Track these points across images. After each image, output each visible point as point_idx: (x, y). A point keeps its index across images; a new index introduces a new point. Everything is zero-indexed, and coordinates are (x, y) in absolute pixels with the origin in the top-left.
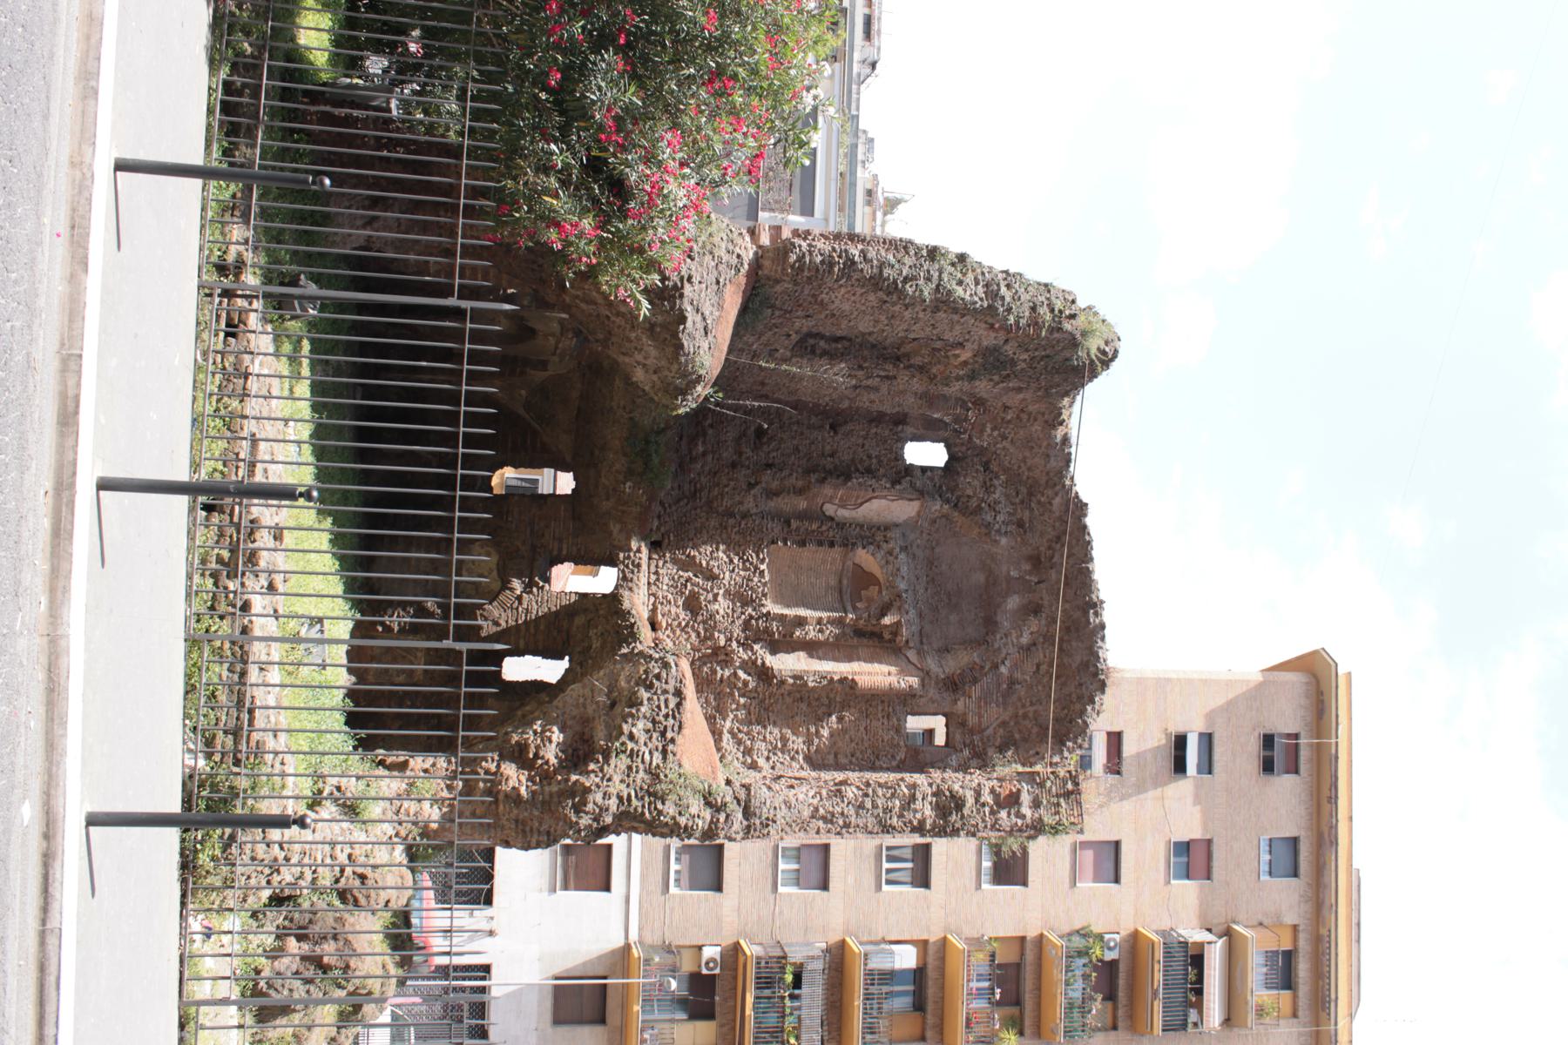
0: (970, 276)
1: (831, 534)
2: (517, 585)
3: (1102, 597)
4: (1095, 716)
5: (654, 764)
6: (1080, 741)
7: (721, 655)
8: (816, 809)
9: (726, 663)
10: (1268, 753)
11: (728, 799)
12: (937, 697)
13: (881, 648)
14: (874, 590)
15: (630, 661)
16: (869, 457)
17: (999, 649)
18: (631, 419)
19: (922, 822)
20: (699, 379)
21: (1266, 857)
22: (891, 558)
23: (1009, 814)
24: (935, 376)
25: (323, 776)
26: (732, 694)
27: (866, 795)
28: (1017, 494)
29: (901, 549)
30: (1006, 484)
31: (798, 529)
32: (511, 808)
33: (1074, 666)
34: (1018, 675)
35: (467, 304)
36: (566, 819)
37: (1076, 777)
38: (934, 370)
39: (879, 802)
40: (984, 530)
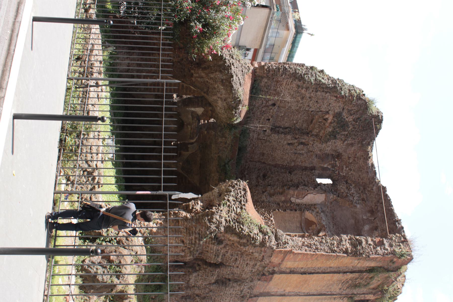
3: (399, 218)
8: (304, 243)
14: (314, 226)
16: (304, 181)
18: (219, 156)
19: (347, 249)
23: (381, 249)
28: (360, 190)
30: (355, 187)
31: (282, 206)
40: (350, 202)
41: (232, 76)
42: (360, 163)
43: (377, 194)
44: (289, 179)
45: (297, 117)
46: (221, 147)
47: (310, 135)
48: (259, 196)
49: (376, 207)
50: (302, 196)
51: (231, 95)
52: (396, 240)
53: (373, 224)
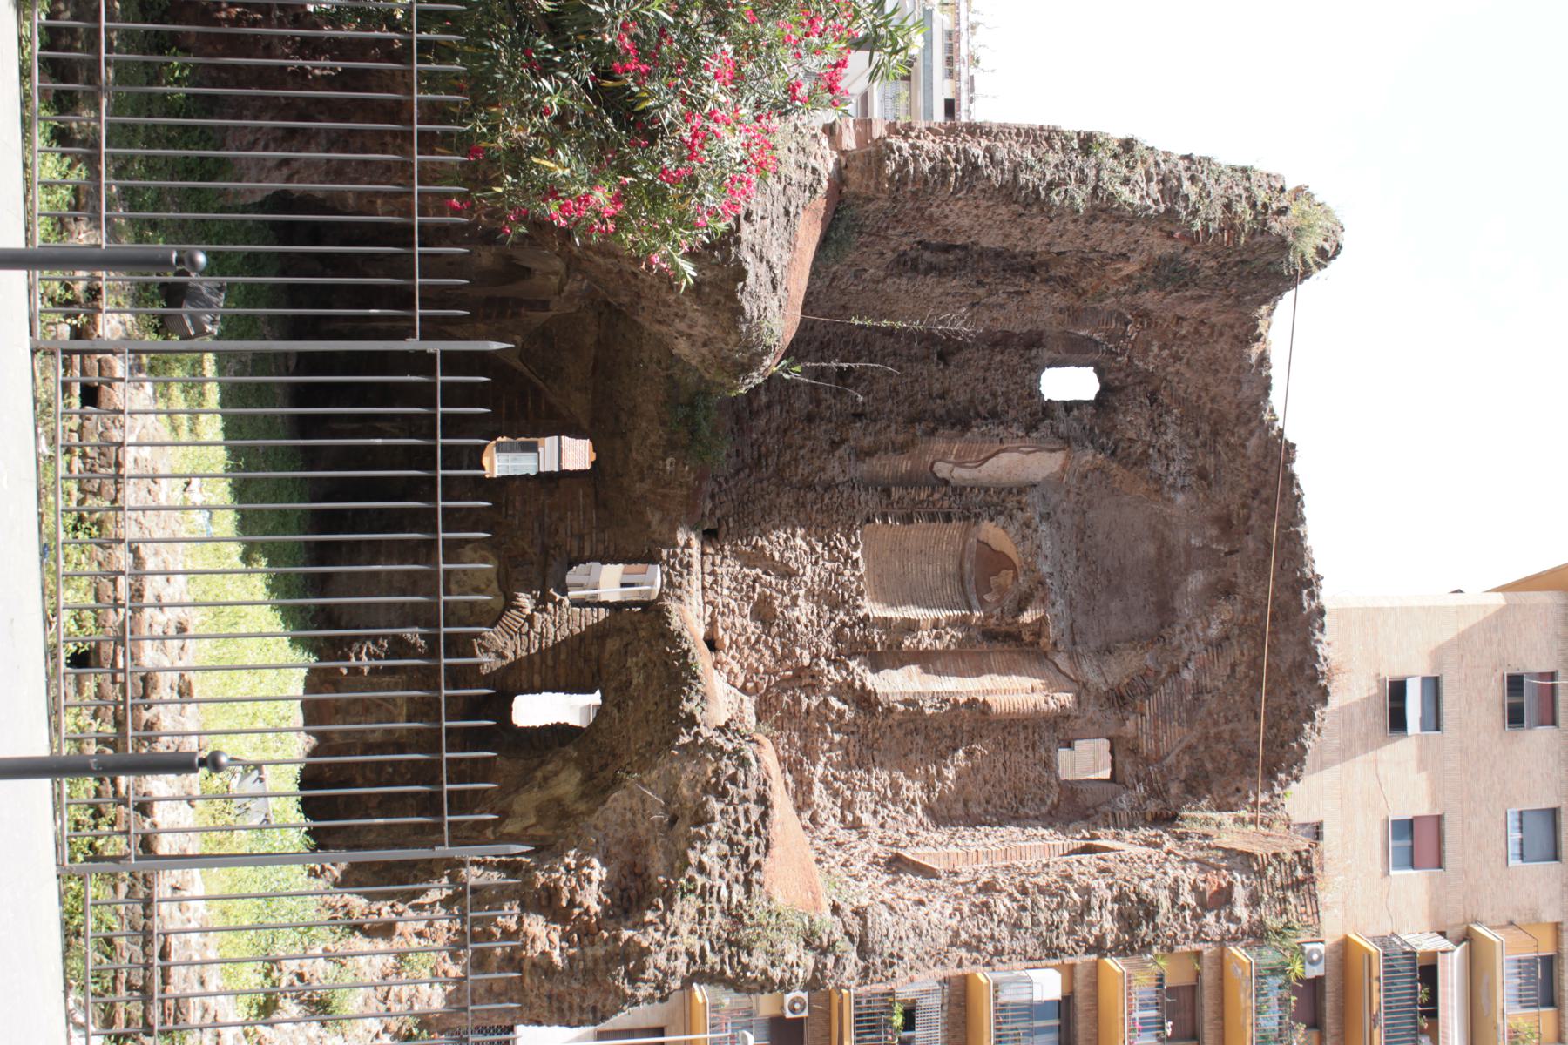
0: (1140, 169)
1: (946, 504)
4: (1315, 736)
5: (734, 901)
6: (1295, 771)
7: (806, 678)
8: (957, 934)
9: (813, 687)
10: (1515, 700)
11: (837, 935)
14: (1006, 577)
15: (693, 756)
16: (994, 395)
17: (1180, 647)
19: (1100, 939)
20: (767, 350)
21: (1515, 836)
22: (1029, 532)
23: (1218, 918)
24: (1085, 292)
25: (275, 961)
26: (822, 730)
27: (1024, 908)
28: (1197, 434)
29: (1042, 517)
31: (901, 499)
32: (541, 982)
34: (1207, 681)
35: (435, 347)
36: (618, 992)
37: (1308, 859)
38: (1083, 284)
39: (1041, 917)
40: (1153, 486)
41: (741, 274)
43: (1257, 465)
44: (937, 387)
47: (1038, 279)
48: (817, 463)
49: (1243, 512)
50: (978, 456)
52: (1278, 878)
53: (1219, 570)
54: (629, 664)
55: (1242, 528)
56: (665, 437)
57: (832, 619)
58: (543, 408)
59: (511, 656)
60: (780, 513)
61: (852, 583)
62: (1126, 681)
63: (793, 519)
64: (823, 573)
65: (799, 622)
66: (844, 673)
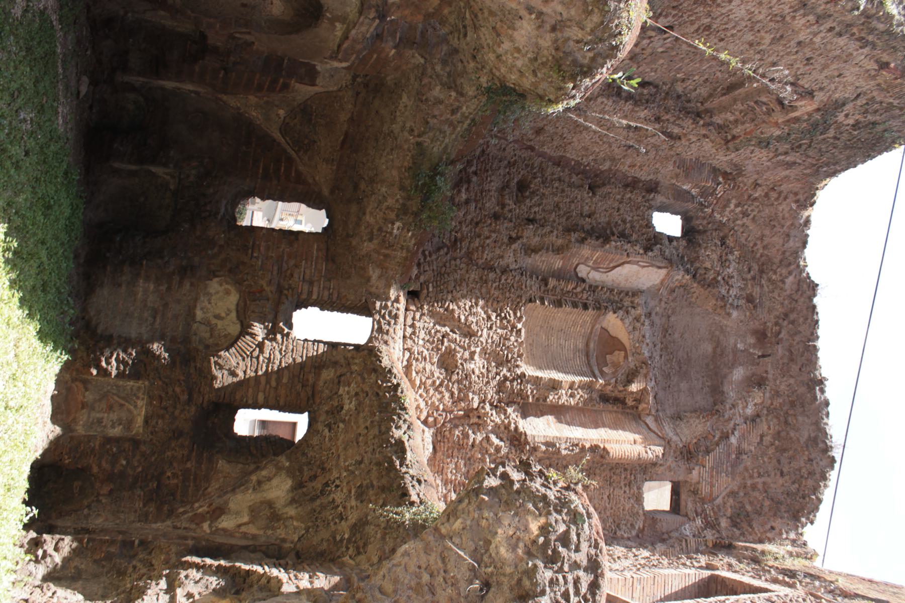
1: (585, 296)
2: (259, 330)
9: (478, 426)
12: (673, 465)
13: (622, 413)
14: (618, 356)
16: (624, 221)
22: (638, 325)
28: (749, 271)
30: (739, 260)
31: (554, 288)
33: (802, 440)
34: (745, 446)
40: (720, 303)
42: (780, 208)
43: (790, 297)
45: (697, 65)
46: (434, 117)
50: (609, 264)
51: (596, 18)
53: (754, 368)
54: (341, 392)
55: (773, 340)
56: (401, 201)
57: (497, 374)
58: (293, 174)
59: (241, 375)
60: (467, 286)
61: (515, 347)
62: (695, 441)
63: (477, 291)
64: (495, 336)
65: (473, 373)
66: (503, 417)
